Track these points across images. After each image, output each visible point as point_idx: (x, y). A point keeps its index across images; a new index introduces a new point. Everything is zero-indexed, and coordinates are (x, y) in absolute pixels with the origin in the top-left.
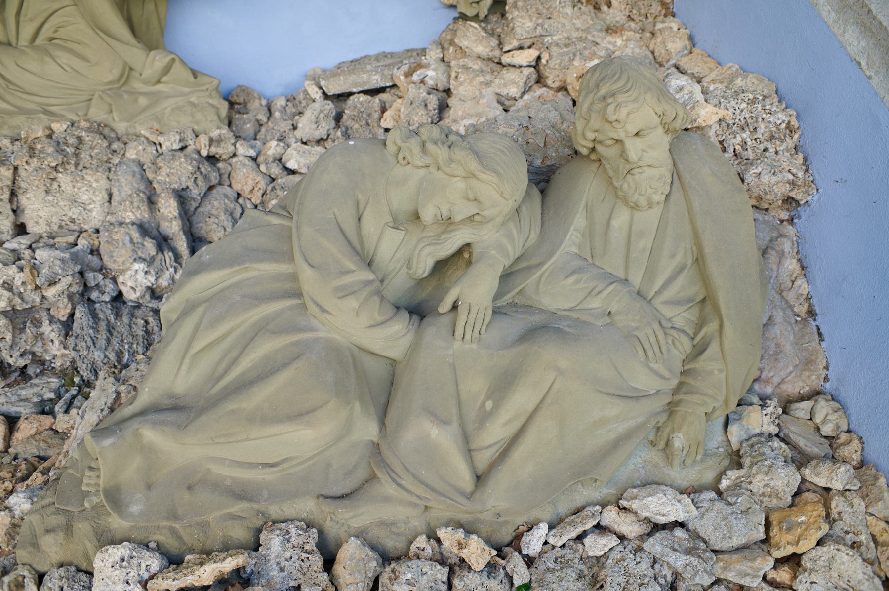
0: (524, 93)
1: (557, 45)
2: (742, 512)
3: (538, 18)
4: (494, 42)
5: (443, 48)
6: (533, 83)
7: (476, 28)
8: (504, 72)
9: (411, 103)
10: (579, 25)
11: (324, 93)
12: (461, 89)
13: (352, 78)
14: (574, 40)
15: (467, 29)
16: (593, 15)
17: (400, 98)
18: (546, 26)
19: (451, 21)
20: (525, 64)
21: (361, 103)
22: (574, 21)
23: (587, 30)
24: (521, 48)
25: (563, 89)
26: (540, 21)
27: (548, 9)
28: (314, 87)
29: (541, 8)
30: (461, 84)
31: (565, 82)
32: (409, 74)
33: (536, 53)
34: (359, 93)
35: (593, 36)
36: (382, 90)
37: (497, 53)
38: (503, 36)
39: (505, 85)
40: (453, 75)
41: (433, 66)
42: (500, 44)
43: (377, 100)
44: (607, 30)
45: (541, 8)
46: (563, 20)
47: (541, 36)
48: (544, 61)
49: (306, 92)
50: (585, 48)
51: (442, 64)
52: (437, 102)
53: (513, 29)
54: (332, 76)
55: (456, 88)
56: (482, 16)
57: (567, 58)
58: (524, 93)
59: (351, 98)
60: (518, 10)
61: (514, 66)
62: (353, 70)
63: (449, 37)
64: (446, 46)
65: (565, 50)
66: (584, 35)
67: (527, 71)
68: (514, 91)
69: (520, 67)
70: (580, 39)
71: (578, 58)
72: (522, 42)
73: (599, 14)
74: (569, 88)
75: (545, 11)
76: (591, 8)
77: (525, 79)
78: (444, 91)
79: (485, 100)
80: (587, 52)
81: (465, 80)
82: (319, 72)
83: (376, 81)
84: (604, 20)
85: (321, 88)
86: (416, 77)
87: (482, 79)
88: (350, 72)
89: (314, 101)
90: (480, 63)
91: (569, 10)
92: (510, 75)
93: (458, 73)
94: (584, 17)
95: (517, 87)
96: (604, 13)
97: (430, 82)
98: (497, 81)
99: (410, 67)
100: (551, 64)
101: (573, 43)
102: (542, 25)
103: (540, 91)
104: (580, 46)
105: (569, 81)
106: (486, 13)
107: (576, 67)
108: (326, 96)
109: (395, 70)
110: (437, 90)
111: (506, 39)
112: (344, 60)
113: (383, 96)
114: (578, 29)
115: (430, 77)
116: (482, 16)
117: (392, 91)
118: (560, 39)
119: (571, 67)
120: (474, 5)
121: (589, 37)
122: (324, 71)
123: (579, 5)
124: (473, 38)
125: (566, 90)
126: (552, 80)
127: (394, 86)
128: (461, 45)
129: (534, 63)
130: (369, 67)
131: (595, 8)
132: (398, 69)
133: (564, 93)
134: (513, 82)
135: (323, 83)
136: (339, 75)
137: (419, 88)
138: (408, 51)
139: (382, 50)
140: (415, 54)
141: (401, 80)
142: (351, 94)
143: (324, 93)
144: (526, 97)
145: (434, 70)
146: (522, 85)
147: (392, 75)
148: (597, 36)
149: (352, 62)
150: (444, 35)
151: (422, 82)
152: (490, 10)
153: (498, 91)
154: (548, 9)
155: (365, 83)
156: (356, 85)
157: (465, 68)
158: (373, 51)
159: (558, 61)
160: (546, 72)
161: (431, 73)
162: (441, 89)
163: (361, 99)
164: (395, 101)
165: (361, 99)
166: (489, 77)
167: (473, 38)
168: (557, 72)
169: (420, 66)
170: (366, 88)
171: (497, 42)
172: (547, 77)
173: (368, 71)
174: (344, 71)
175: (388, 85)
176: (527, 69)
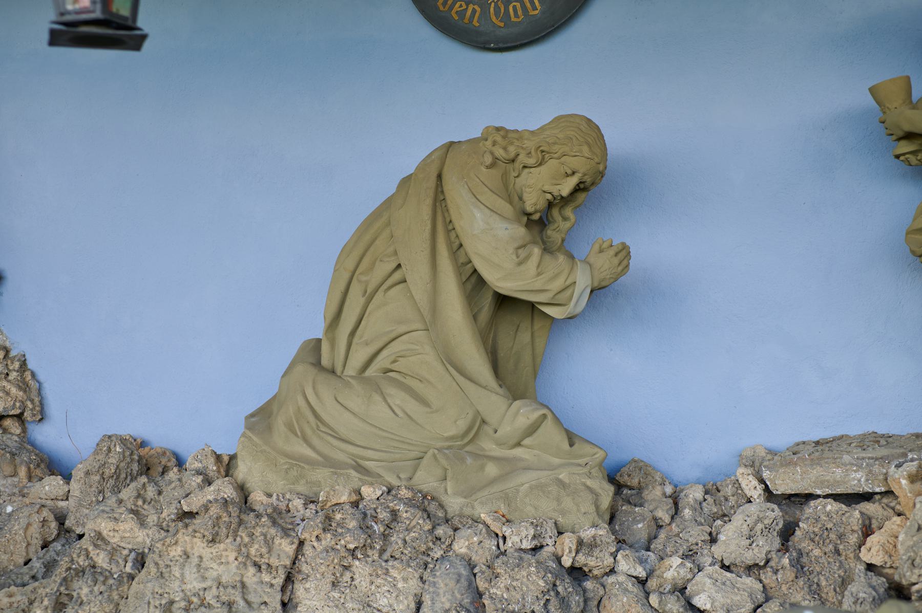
11: (767, 489)
13: (816, 472)
17: (899, 515)
28: (751, 478)
34: (826, 496)
36: (867, 497)
43: (857, 514)
49: (737, 484)
54: (782, 465)
85: (762, 481)
88: (814, 462)
113: (869, 508)
117: (885, 500)
122: (772, 452)
127: (889, 493)
130: (846, 458)
132: (898, 466)
135: (766, 474)
136: (796, 464)
143: (767, 489)
147: (886, 474)
149: (817, 443)
155: (837, 483)
156: (821, 483)
158: (855, 430)
163: (829, 508)
165: (829, 508)
170: (839, 490)
173: (845, 465)
174: (803, 459)
175: (878, 490)
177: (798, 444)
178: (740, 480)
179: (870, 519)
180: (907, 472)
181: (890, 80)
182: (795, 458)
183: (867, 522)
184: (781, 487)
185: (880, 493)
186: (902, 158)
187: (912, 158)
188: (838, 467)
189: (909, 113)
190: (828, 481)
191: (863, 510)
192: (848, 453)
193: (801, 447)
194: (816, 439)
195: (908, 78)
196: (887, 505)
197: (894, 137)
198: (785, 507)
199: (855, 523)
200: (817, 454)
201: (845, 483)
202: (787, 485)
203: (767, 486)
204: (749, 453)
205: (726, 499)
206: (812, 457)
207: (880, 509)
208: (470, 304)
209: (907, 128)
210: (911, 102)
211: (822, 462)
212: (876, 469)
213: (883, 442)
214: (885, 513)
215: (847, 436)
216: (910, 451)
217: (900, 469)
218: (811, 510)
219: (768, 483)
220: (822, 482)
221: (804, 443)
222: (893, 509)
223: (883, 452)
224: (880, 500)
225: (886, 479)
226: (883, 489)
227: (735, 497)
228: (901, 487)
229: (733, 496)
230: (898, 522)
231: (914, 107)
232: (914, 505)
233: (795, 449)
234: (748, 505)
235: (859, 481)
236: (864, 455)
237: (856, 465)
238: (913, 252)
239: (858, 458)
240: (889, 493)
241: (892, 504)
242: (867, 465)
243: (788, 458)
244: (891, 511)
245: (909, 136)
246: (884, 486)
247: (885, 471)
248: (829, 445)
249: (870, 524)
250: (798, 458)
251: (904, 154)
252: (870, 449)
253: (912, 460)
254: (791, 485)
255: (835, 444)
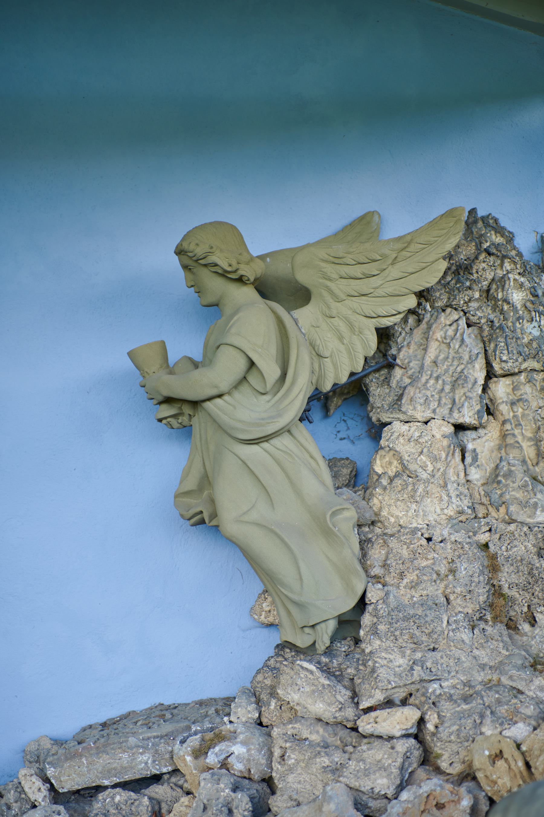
0: (401, 788)
1: (450, 698)
2: (419, 372)
3: (414, 651)
4: (344, 695)
5: (258, 702)
6: (415, 765)
7: (311, 672)
8: (364, 747)
9: (205, 808)
10: (486, 660)
11: (52, 789)
12: (291, 778)
13: (103, 761)
14: (479, 688)
15: (298, 674)
16: (506, 639)
17: (188, 793)
18: (429, 664)
19: (272, 652)
20: (398, 734)
21: (117, 807)
22: (476, 652)
23: (498, 668)
24: (389, 703)
25: (468, 776)
26: (418, 655)
27: (429, 635)
28: (34, 779)
29: (417, 633)
30: (291, 770)
31: (470, 766)
32: (200, 753)
33: (415, 715)
34: (115, 786)
35: (511, 678)
36: (156, 779)
37: (350, 712)
38: (357, 681)
39: (367, 773)
40: (277, 752)
41: (241, 737)
42: (355, 696)
43: (146, 801)
44: (533, 666)
45: (417, 633)
46: (457, 653)
47: (422, 681)
48: (430, 727)
49: (20, 789)
50: (499, 702)
51: (257, 731)
52: (249, 806)
53: (373, 671)
54: (67, 759)
55: (283, 777)
56: (321, 647)
57: (469, 723)
58: (401, 788)
59: (100, 796)
60: (380, 639)
61: (380, 737)
62: (105, 746)
63: (268, 682)
64: (264, 697)
65: (465, 707)
66: (495, 677)
67: (402, 746)
68: (383, 783)
69: (391, 738)
70: (488, 685)
71: (488, 720)
72: (389, 693)
73: (517, 637)
74: (480, 775)
75: (424, 638)
76: (501, 627)
77: (400, 760)
78: (264, 780)
79: (332, 806)
80: (503, 710)
81: (298, 761)
82: (47, 744)
83: (144, 763)
84: (526, 648)
85: (46, 780)
86: (212, 759)
87: (326, 761)
88: (100, 751)
89: (34, 806)
90: (321, 731)
91: (465, 635)
92: (376, 753)
93: (284, 750)
94: (493, 644)
95: (388, 776)
96: (526, 634)
97: (238, 767)
98: (352, 764)
99: (203, 740)
100: (444, 734)
101: (477, 693)
102: (422, 663)
103: (429, 785)
104: (490, 698)
105: (477, 764)
106: (328, 643)
107: (488, 738)
108: (56, 796)
109: (177, 746)
110: (250, 779)
111: (364, 688)
112: (92, 721)
113: (158, 791)
114: (483, 667)
115: (238, 757)
116: (321, 647)
117: (173, 780)
118: (454, 687)
119: (479, 738)
120: (307, 630)
121: (504, 680)
122: (58, 742)
123: (482, 625)
124: (307, 689)
125: (474, 778)
126: (448, 759)
127: (176, 771)
128: (288, 698)
129: (413, 731)
130: (132, 740)
131: (508, 627)
132: (183, 742)
133: (472, 784)
134: (381, 768)
135: (50, 772)
136: (81, 756)
137: (218, 781)
138: (201, 703)
139: (157, 701)
140: (212, 711)
141: (187, 761)
142: (99, 788)
143: (52, 789)
144: (404, 796)
145: (244, 743)
146: (395, 771)
147: (172, 752)
148: (519, 678)
149: (104, 725)
150: (260, 678)
151: (224, 765)
152: (333, 640)
153: (354, 783)
154: (429, 635)
155: (125, 769)
156: (108, 773)
157: (297, 740)
158: (141, 704)
159: (455, 728)
160: (437, 748)
161: (238, 749)
162: (256, 777)
163: (118, 798)
164: (177, 800)
165: (118, 798)
166: (338, 757)
167: (307, 689)
168: (455, 747)
169: (220, 738)
170: (127, 777)
171: (349, 693)
172: (439, 756)
173: (131, 748)
174: (88, 749)
175: (165, 770)
176: (402, 741)
177: (84, 730)
178: (23, 783)
179: (159, 803)
180: (191, 747)
181: (146, 345)
182: (80, 748)
183: (157, 808)
184: (68, 782)
185: (169, 773)
186: (164, 421)
187: (172, 421)
188: (125, 751)
189: (166, 378)
190: (115, 769)
191: (153, 795)
192: (134, 734)
193: (88, 732)
194: (103, 720)
195: (163, 343)
196: (176, 785)
197: (155, 402)
198: (73, 805)
199: (145, 811)
200: (102, 740)
201: (132, 768)
202: (73, 780)
203: (52, 785)
204: (34, 747)
205: (9, 808)
206: (97, 745)
207: (169, 790)
208: (216, 511)
209: (166, 393)
210: (168, 366)
211: (108, 749)
212: (162, 748)
213: (168, 716)
214: (174, 794)
215: (134, 712)
216: (194, 723)
217: (185, 745)
218: (99, 805)
219: (53, 781)
220: (109, 771)
221: (90, 727)
222: (181, 787)
223: (167, 728)
224: (169, 779)
225: (172, 758)
226: (170, 769)
227: (19, 803)
228: (186, 765)
229: (16, 802)
230: (186, 803)
231: (171, 372)
232: (199, 783)
233: (80, 738)
234: (31, 812)
235: (146, 763)
236: (149, 735)
237: (142, 747)
238: (182, 516)
239: (143, 739)
240: (176, 771)
241: (180, 783)
242: (153, 745)
243: (72, 750)
244: (179, 790)
245: (168, 400)
246: (170, 765)
247: (170, 748)
248: (115, 726)
249: (160, 809)
250: (83, 748)
251: (165, 418)
252: (155, 726)
253: (196, 733)
254: (78, 779)
255: (122, 723)
